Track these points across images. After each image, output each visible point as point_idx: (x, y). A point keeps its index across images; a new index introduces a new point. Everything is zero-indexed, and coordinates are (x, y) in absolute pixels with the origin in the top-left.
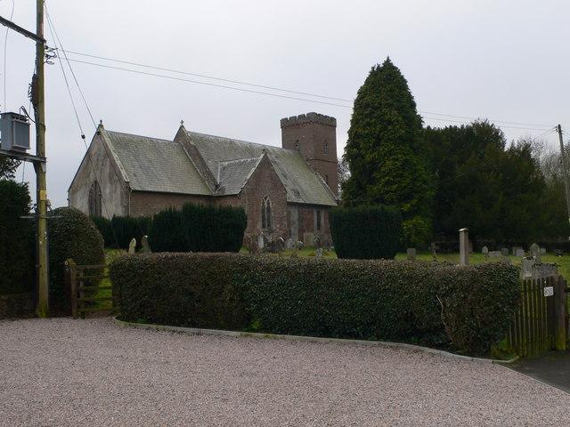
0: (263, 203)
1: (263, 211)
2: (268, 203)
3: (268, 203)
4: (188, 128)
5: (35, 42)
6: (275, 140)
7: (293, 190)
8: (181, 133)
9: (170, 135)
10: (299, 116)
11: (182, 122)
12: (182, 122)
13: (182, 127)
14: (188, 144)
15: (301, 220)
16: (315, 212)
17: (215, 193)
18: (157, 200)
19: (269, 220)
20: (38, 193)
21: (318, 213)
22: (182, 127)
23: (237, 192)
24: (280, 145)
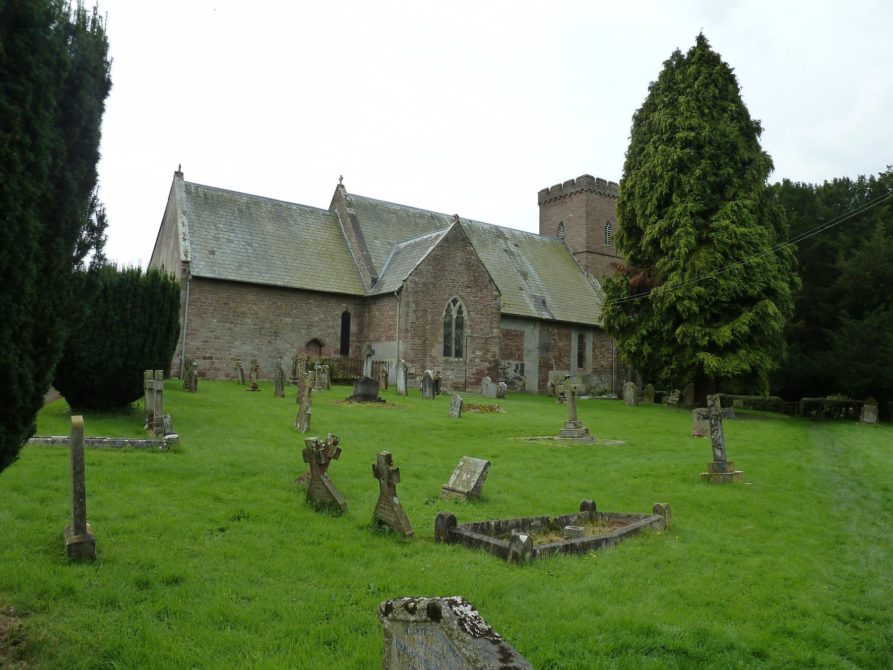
0: (448, 311)
1: (448, 325)
2: (460, 312)
3: (460, 312)
4: (352, 189)
5: (696, 45)
6: (527, 219)
7: (534, 297)
8: (340, 197)
9: (324, 202)
10: (566, 183)
11: (341, 178)
12: (341, 178)
13: (340, 186)
14: (350, 215)
15: (544, 348)
16: (574, 336)
17: (371, 292)
18: (205, 288)
19: (458, 342)
20: (488, 544)
21: (581, 338)
22: (340, 186)
23: (395, 288)
24: (533, 227)
